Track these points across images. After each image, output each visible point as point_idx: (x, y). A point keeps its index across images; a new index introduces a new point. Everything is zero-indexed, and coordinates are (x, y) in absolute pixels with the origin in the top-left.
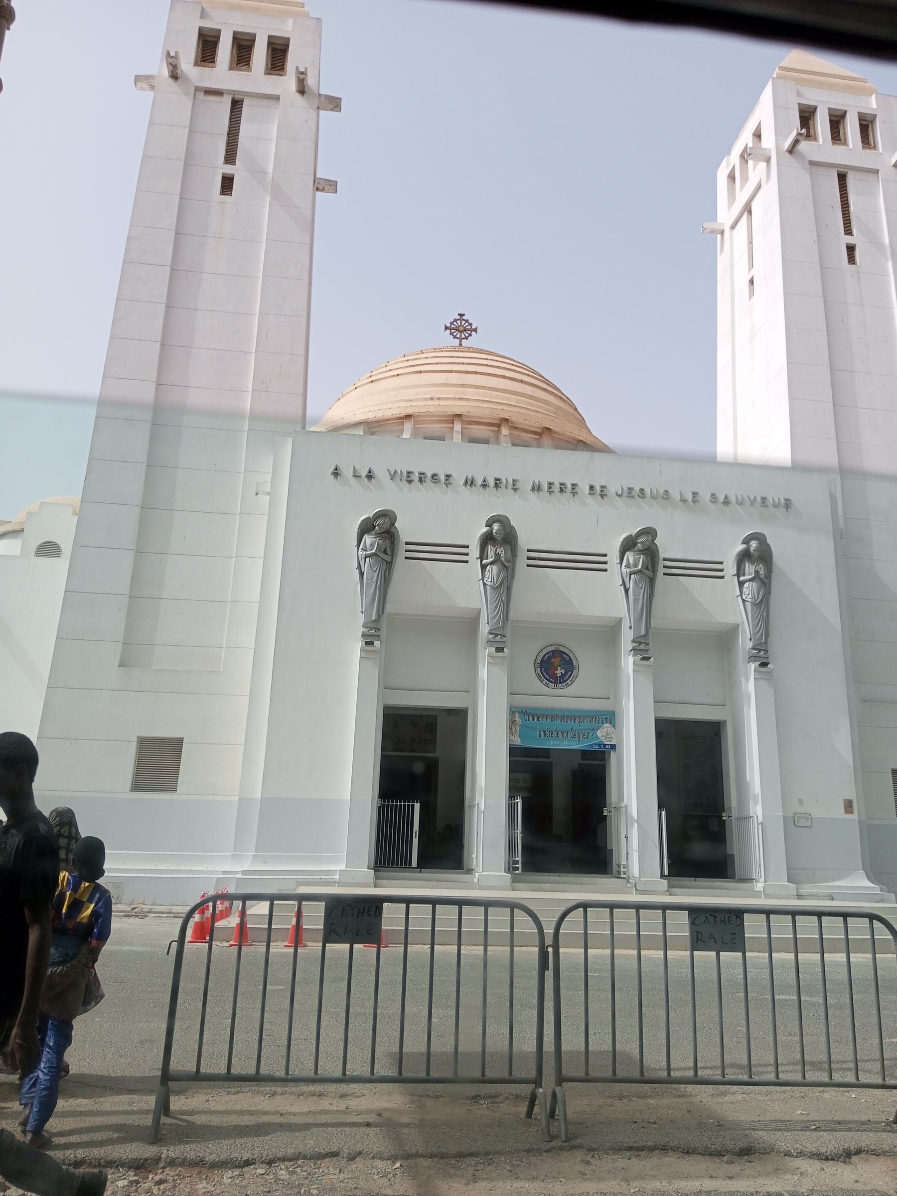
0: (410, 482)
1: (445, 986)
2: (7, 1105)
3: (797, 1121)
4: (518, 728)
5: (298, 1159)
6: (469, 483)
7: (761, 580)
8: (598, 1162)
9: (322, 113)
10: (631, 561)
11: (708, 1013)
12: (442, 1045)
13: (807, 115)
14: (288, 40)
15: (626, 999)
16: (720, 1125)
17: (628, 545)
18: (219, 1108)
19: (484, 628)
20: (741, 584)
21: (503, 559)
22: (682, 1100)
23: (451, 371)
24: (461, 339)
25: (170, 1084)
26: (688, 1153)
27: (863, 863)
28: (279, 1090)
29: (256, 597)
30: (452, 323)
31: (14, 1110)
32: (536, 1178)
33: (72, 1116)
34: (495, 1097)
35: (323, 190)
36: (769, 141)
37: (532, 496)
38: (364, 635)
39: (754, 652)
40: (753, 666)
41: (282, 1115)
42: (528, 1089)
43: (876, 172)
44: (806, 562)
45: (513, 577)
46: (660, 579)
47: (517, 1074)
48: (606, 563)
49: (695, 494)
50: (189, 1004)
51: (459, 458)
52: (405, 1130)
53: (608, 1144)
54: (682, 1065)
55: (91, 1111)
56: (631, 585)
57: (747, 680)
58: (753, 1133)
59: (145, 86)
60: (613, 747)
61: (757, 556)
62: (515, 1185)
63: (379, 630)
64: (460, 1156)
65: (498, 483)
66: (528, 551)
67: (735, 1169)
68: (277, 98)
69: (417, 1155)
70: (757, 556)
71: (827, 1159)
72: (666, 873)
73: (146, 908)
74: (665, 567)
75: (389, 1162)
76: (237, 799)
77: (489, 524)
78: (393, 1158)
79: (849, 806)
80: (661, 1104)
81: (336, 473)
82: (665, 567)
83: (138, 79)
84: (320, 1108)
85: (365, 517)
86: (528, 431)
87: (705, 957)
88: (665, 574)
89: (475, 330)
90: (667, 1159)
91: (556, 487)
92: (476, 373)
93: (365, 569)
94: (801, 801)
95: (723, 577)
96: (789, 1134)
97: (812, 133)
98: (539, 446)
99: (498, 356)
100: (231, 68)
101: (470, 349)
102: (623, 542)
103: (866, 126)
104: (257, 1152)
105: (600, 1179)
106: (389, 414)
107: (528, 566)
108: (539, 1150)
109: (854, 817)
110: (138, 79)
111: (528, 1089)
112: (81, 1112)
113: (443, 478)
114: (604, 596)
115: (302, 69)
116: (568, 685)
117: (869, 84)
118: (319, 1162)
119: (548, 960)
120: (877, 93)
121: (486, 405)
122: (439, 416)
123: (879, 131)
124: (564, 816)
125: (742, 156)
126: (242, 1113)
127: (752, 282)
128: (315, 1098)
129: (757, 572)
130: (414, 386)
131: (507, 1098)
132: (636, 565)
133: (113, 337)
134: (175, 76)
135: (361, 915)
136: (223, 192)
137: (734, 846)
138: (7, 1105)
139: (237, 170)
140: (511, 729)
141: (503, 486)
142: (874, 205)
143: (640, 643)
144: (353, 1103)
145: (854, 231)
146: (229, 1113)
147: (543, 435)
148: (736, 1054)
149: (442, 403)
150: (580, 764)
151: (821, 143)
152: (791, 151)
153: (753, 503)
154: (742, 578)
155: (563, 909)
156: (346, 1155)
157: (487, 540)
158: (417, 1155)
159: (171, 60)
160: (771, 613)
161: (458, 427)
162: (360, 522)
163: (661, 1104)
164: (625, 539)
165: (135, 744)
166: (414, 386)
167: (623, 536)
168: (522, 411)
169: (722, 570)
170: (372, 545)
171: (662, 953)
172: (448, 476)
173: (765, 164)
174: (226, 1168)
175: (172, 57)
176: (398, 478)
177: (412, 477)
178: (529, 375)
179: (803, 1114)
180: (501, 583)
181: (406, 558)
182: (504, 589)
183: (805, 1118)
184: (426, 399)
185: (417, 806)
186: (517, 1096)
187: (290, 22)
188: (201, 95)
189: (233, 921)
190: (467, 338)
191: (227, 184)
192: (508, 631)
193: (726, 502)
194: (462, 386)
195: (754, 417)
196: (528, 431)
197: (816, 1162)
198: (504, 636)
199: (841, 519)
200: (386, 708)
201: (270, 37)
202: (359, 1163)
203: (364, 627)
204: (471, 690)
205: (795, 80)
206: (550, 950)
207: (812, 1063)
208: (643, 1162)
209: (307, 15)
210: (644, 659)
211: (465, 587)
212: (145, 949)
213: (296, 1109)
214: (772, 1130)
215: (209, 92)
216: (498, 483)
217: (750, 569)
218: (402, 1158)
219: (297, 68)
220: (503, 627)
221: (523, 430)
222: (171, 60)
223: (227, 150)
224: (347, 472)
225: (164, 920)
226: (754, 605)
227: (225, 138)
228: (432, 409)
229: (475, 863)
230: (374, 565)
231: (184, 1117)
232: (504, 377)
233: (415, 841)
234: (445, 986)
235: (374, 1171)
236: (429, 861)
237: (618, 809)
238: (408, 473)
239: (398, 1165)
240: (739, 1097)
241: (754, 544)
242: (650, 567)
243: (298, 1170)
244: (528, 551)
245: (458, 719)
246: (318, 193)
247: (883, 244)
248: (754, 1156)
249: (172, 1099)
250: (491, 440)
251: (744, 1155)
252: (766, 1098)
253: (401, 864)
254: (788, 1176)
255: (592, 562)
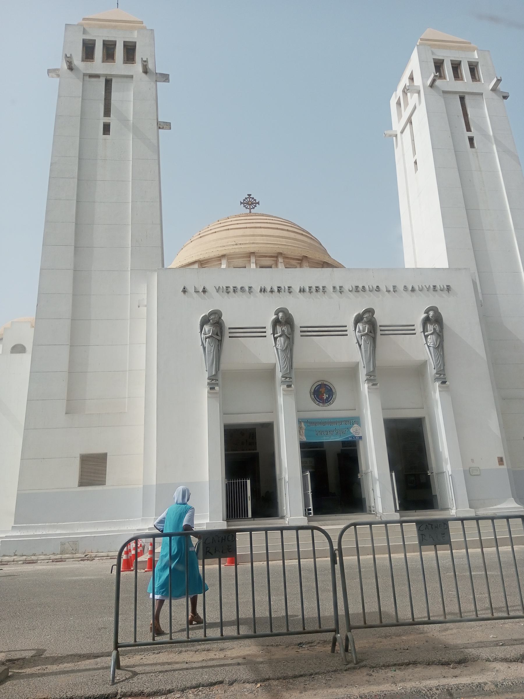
0: (228, 293)
1: (277, 583)
2: (22, 671)
3: (491, 642)
4: (304, 431)
5: (199, 687)
6: (263, 290)
7: (438, 334)
8: (377, 674)
9: (158, 83)
10: (361, 329)
11: (433, 585)
12: (279, 612)
13: (438, 65)
14: (135, 43)
15: (385, 582)
16: (446, 647)
17: (358, 319)
18: (149, 662)
19: (279, 375)
20: (426, 337)
21: (286, 333)
22: (422, 635)
23: (246, 228)
24: (250, 209)
25: (119, 649)
26: (429, 664)
27: (512, 493)
28: (184, 649)
29: (144, 367)
30: (244, 200)
31: (27, 673)
32: (342, 686)
33: (62, 674)
34: (312, 643)
35: (163, 128)
36: (418, 81)
37: (300, 295)
38: (209, 384)
39: (437, 375)
40: (437, 384)
41: (187, 663)
42: (330, 636)
43: (482, 94)
44: (462, 320)
45: (293, 343)
46: (379, 337)
47: (324, 627)
48: (346, 331)
49: (394, 287)
50: (126, 606)
51: (254, 276)
52: (260, 665)
53: (381, 664)
54: (419, 616)
55: (73, 670)
56: (362, 343)
57: (435, 392)
58: (466, 650)
59: (54, 75)
60: (361, 438)
61: (434, 320)
62: (329, 691)
63: (217, 380)
64: (295, 677)
65: (279, 289)
66: (301, 327)
67: (457, 671)
68: (132, 77)
69: (268, 679)
70: (434, 320)
71: (511, 661)
72: (398, 509)
73: (93, 555)
74: (381, 330)
75: (254, 684)
76: (142, 486)
77: (277, 313)
78: (256, 682)
79: (501, 461)
80: (410, 638)
81: (184, 291)
82: (381, 330)
83: (49, 71)
84: (209, 658)
85: (204, 315)
86: (294, 259)
87: (429, 553)
88: (381, 335)
89: (258, 203)
90: (416, 669)
91: (314, 289)
92: (261, 228)
93: (206, 345)
94: (472, 460)
95: (415, 334)
96: (487, 649)
97: (442, 75)
98: (301, 267)
99: (273, 217)
100: (103, 62)
101: (256, 214)
102: (355, 318)
103: (473, 69)
104: (174, 685)
105: (379, 684)
106: (212, 255)
107: (301, 336)
108: (341, 670)
109: (505, 467)
110: (49, 71)
111: (330, 636)
112: (67, 671)
113: (247, 289)
114: (348, 350)
115: (145, 59)
116: (331, 404)
117: (472, 45)
118: (212, 688)
119: (336, 555)
120: (477, 50)
121: (268, 246)
122: (241, 254)
123: (481, 71)
124: (335, 480)
125: (404, 91)
126: (163, 664)
127: (416, 163)
128: (205, 652)
129: (434, 329)
130: (226, 238)
131: (319, 643)
132: (364, 331)
133: (47, 222)
134: (71, 68)
135: (224, 538)
136: (104, 133)
137: (436, 490)
138: (22, 671)
139: (113, 120)
140: (300, 432)
141: (283, 291)
142: (483, 113)
143: (371, 376)
144: (229, 653)
145: (472, 129)
146: (156, 664)
147: (302, 261)
148: (452, 607)
149: (242, 246)
150: (341, 450)
151: (448, 80)
152: (432, 86)
153: (428, 289)
154: (426, 334)
155: (338, 534)
156: (227, 682)
157: (276, 323)
158: (268, 679)
159: (68, 59)
160: (445, 352)
161: (253, 260)
162: (201, 318)
163: (410, 638)
164: (356, 316)
165: (79, 459)
166: (226, 238)
167: (355, 315)
168: (290, 247)
169: (414, 330)
170: (209, 331)
171: (356, 557)
172: (250, 288)
173: (417, 95)
174: (157, 695)
175: (68, 57)
176: (221, 291)
177: (229, 290)
178: (292, 227)
179: (494, 637)
180: (287, 347)
181: (230, 337)
182: (289, 350)
183: (495, 639)
184: (233, 245)
185: (249, 482)
186: (325, 642)
187: (136, 33)
188: (87, 78)
189: (145, 558)
190: (254, 208)
191: (107, 129)
192: (293, 375)
193: (413, 290)
194: (253, 235)
195: (424, 241)
196: (294, 259)
197: (505, 663)
198: (291, 378)
199: (480, 295)
200: (225, 426)
201: (124, 42)
202: (236, 686)
203: (208, 379)
204: (274, 411)
205: (430, 45)
206: (337, 552)
207: (495, 608)
208: (403, 673)
209: (145, 28)
210: (373, 385)
211: (266, 351)
212: (96, 577)
213: (195, 659)
214: (477, 648)
215: (91, 76)
216: (279, 289)
217: (430, 328)
218: (261, 681)
219: (142, 58)
220: (290, 373)
221: (291, 258)
222: (68, 59)
223: (105, 109)
224: (191, 290)
225: (104, 561)
226: (435, 348)
227: (103, 101)
228: (237, 250)
229: (285, 511)
230: (212, 343)
231: (129, 669)
232: (277, 229)
233: (249, 503)
234: (277, 583)
235: (245, 690)
236: (256, 514)
237: (366, 474)
238: (227, 287)
239: (259, 685)
240: (455, 631)
241: (431, 313)
242: (372, 331)
243: (200, 693)
244: (301, 327)
245: (268, 429)
246: (160, 130)
247: (489, 135)
248: (468, 663)
249: (121, 658)
250: (273, 266)
251: (462, 663)
252: (471, 630)
253: (242, 517)
254: (489, 673)
255: (339, 331)
